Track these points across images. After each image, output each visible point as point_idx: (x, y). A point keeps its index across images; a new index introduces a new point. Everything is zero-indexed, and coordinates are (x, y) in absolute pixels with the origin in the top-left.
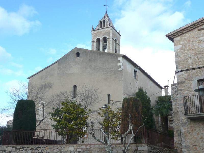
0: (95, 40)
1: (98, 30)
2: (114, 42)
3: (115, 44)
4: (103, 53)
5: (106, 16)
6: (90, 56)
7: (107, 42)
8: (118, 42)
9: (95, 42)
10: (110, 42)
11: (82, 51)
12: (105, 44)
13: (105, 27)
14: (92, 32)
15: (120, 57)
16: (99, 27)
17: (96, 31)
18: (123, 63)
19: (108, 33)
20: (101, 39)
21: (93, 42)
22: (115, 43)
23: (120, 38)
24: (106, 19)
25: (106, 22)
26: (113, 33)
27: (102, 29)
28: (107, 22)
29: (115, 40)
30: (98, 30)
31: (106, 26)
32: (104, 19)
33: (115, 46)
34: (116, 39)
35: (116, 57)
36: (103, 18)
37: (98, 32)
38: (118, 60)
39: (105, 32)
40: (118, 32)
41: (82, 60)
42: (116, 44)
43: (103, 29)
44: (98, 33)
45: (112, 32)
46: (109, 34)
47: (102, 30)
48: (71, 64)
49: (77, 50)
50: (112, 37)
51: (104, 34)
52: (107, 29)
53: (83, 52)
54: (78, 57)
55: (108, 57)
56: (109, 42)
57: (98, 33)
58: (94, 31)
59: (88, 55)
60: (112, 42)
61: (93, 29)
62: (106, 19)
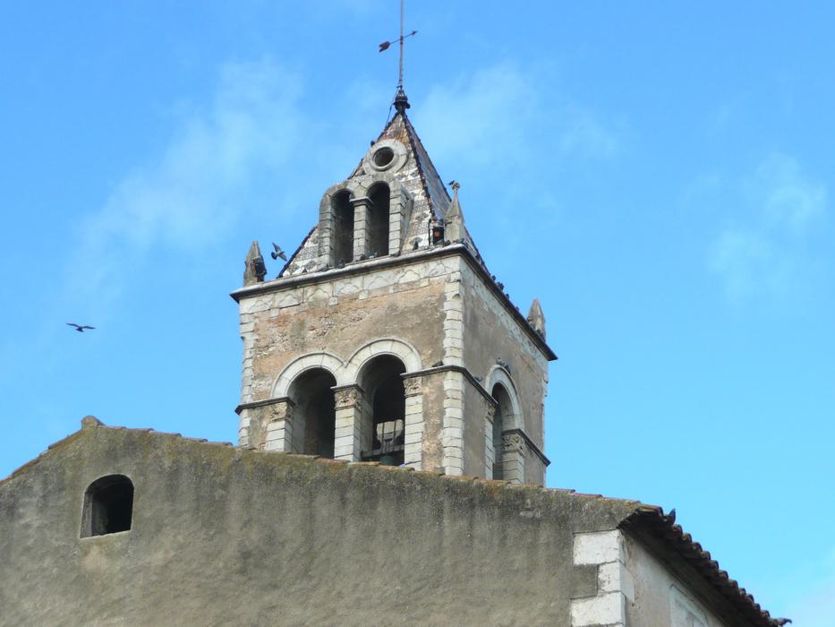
0: (282, 389)
1: (315, 281)
2: (485, 410)
3: (489, 443)
4: (400, 489)
5: (399, 148)
6: (246, 524)
7: (413, 406)
8: (527, 416)
9: (282, 407)
10: (442, 412)
11: (167, 463)
12: (386, 429)
13: (385, 252)
14: (247, 305)
15: (594, 529)
16: (326, 259)
17: (286, 298)
18: (632, 598)
19: (416, 320)
20: (347, 376)
21: (251, 407)
22: (489, 428)
23: (539, 377)
24: (403, 177)
25: (395, 204)
26: (472, 323)
27: (353, 273)
28: (409, 206)
29: (488, 388)
30: (315, 281)
31: (394, 246)
32: (384, 177)
33: (490, 456)
34: (498, 388)
35: (546, 534)
36: (370, 166)
37: (314, 308)
38: (581, 567)
39: (385, 302)
40: (525, 314)
41: (158, 558)
42: (502, 436)
43: (367, 270)
44: (311, 321)
45: (458, 304)
46: (428, 325)
47: (358, 281)
48: (27, 605)
49: (111, 455)
50: (459, 363)
51: (378, 331)
52: (411, 274)
53: (175, 473)
54: (111, 528)
55: (463, 523)
56: (426, 416)
57: (311, 321)
58: (267, 299)
59: (234, 507)
60: (458, 413)
61: (259, 269)
62: (394, 172)
